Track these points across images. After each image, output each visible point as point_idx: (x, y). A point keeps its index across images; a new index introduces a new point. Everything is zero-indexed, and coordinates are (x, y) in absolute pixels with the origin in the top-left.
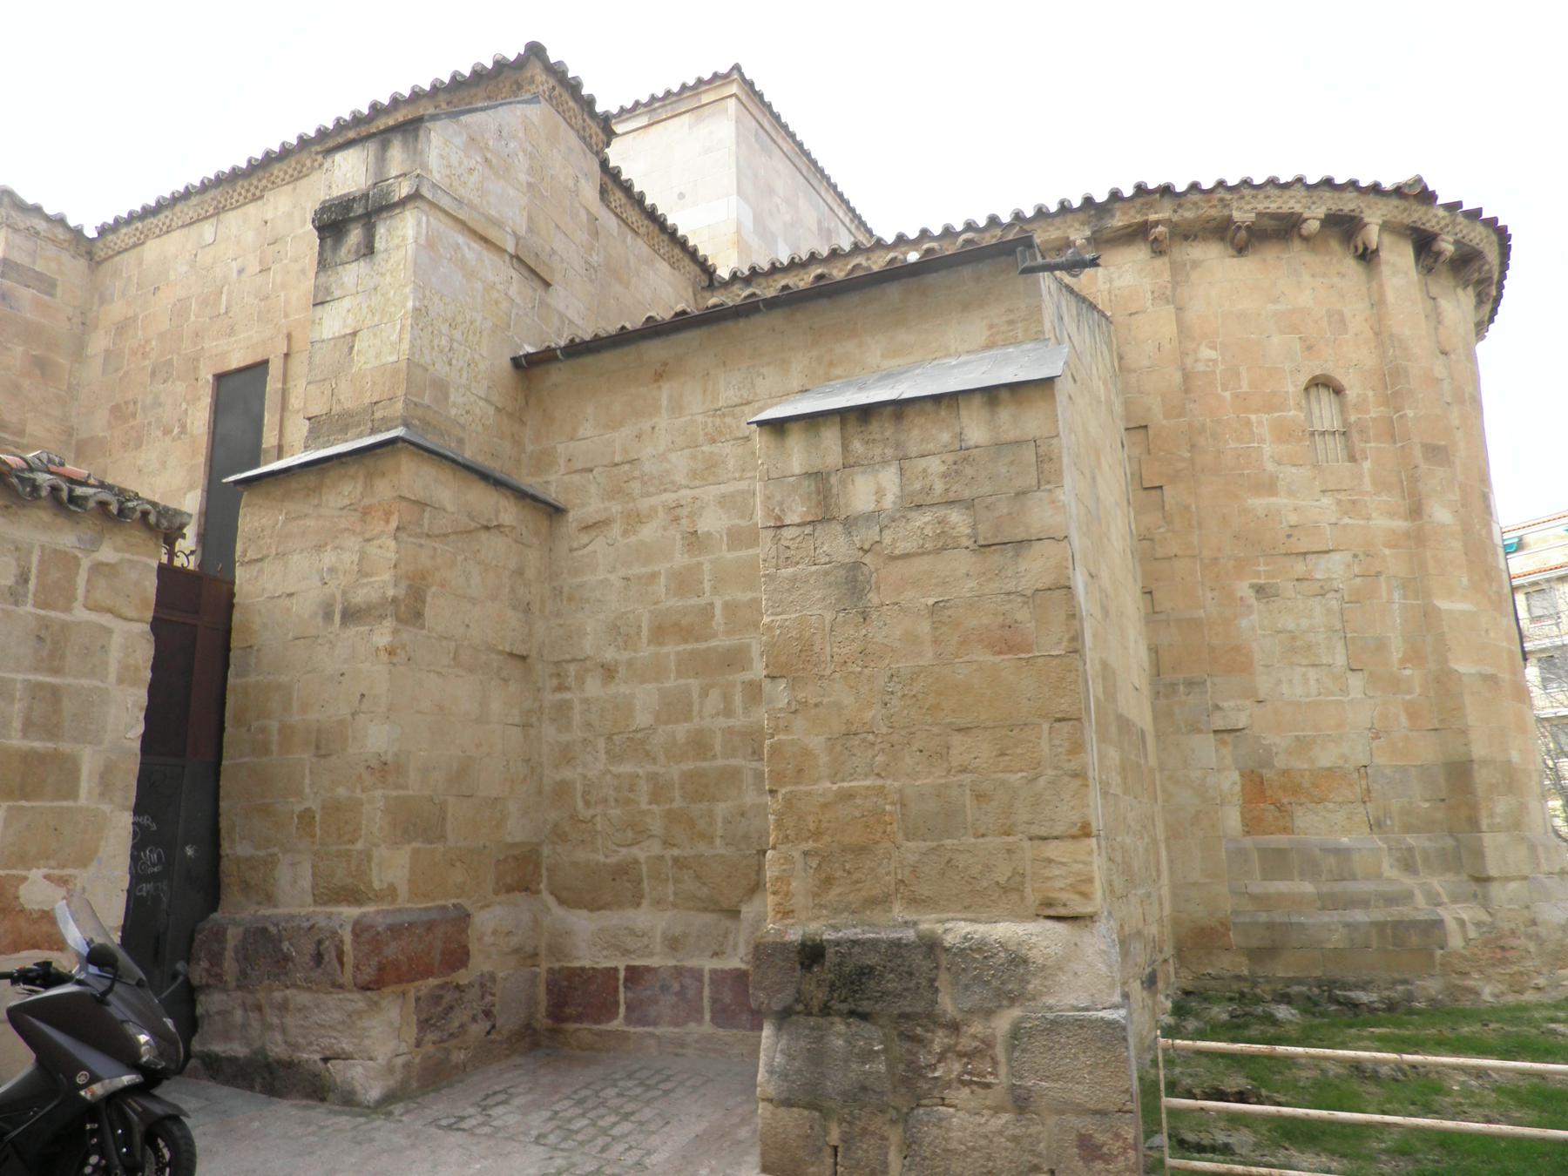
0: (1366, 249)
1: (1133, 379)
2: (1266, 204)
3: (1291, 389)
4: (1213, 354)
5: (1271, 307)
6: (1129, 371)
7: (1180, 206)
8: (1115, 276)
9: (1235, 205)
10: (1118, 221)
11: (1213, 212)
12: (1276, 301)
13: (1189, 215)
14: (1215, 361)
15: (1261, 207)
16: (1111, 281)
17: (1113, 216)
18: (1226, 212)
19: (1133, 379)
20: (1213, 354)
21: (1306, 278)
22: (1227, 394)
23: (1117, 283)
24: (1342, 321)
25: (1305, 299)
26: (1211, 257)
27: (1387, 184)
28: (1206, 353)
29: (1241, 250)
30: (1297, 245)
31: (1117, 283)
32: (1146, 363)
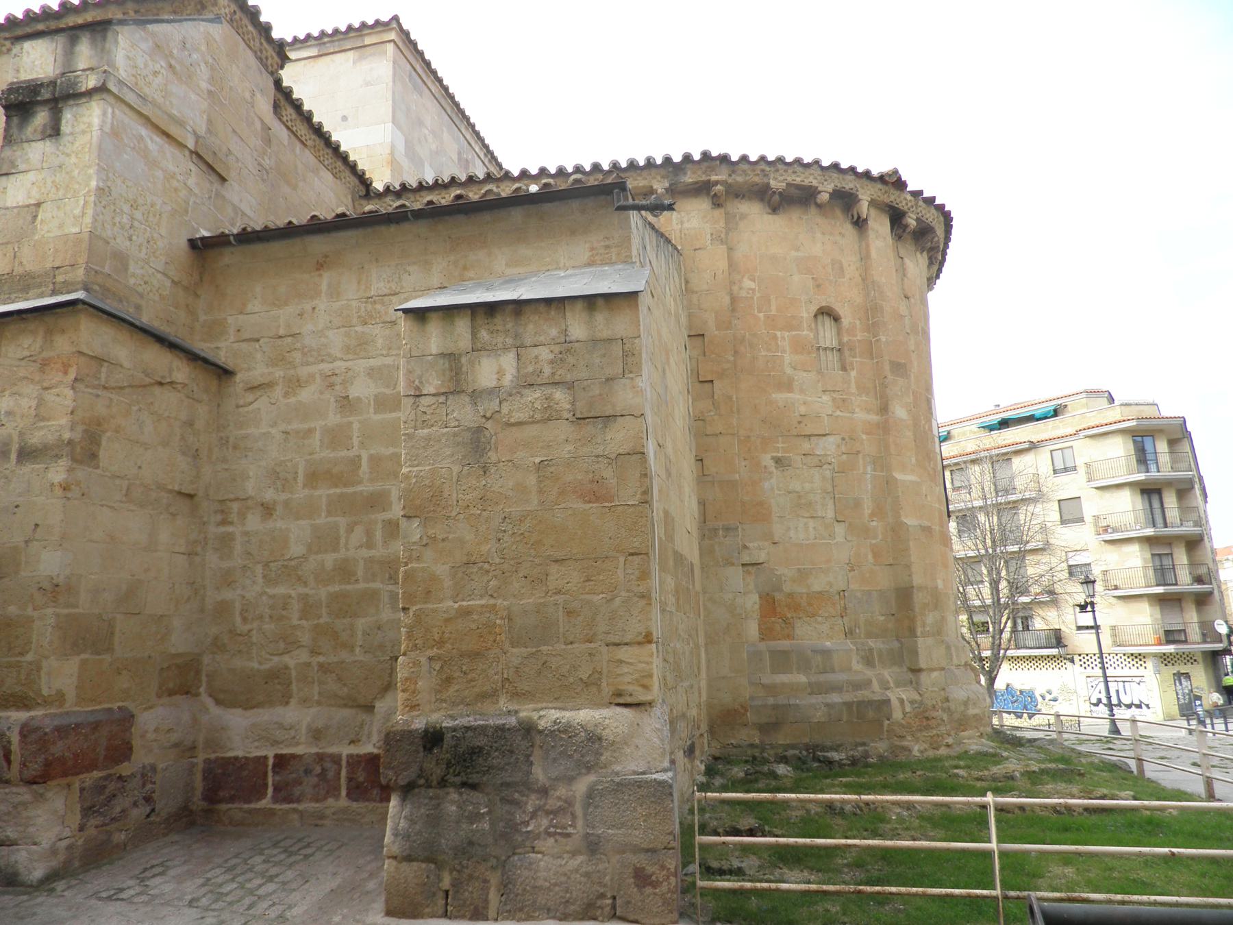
0: (859, 217)
1: (695, 298)
2: (794, 177)
3: (805, 315)
4: (752, 285)
5: (794, 253)
6: (693, 292)
7: (734, 172)
8: (685, 219)
9: (772, 176)
10: (689, 178)
11: (757, 179)
12: (798, 249)
13: (740, 179)
14: (753, 290)
15: (790, 179)
16: (682, 223)
17: (685, 174)
18: (766, 180)
19: (695, 298)
20: (752, 285)
21: (819, 235)
22: (761, 315)
23: (686, 225)
24: (841, 268)
25: (817, 249)
26: (753, 213)
27: (875, 173)
28: (747, 283)
29: (775, 210)
30: (813, 210)
31: (686, 225)
32: (705, 287)
